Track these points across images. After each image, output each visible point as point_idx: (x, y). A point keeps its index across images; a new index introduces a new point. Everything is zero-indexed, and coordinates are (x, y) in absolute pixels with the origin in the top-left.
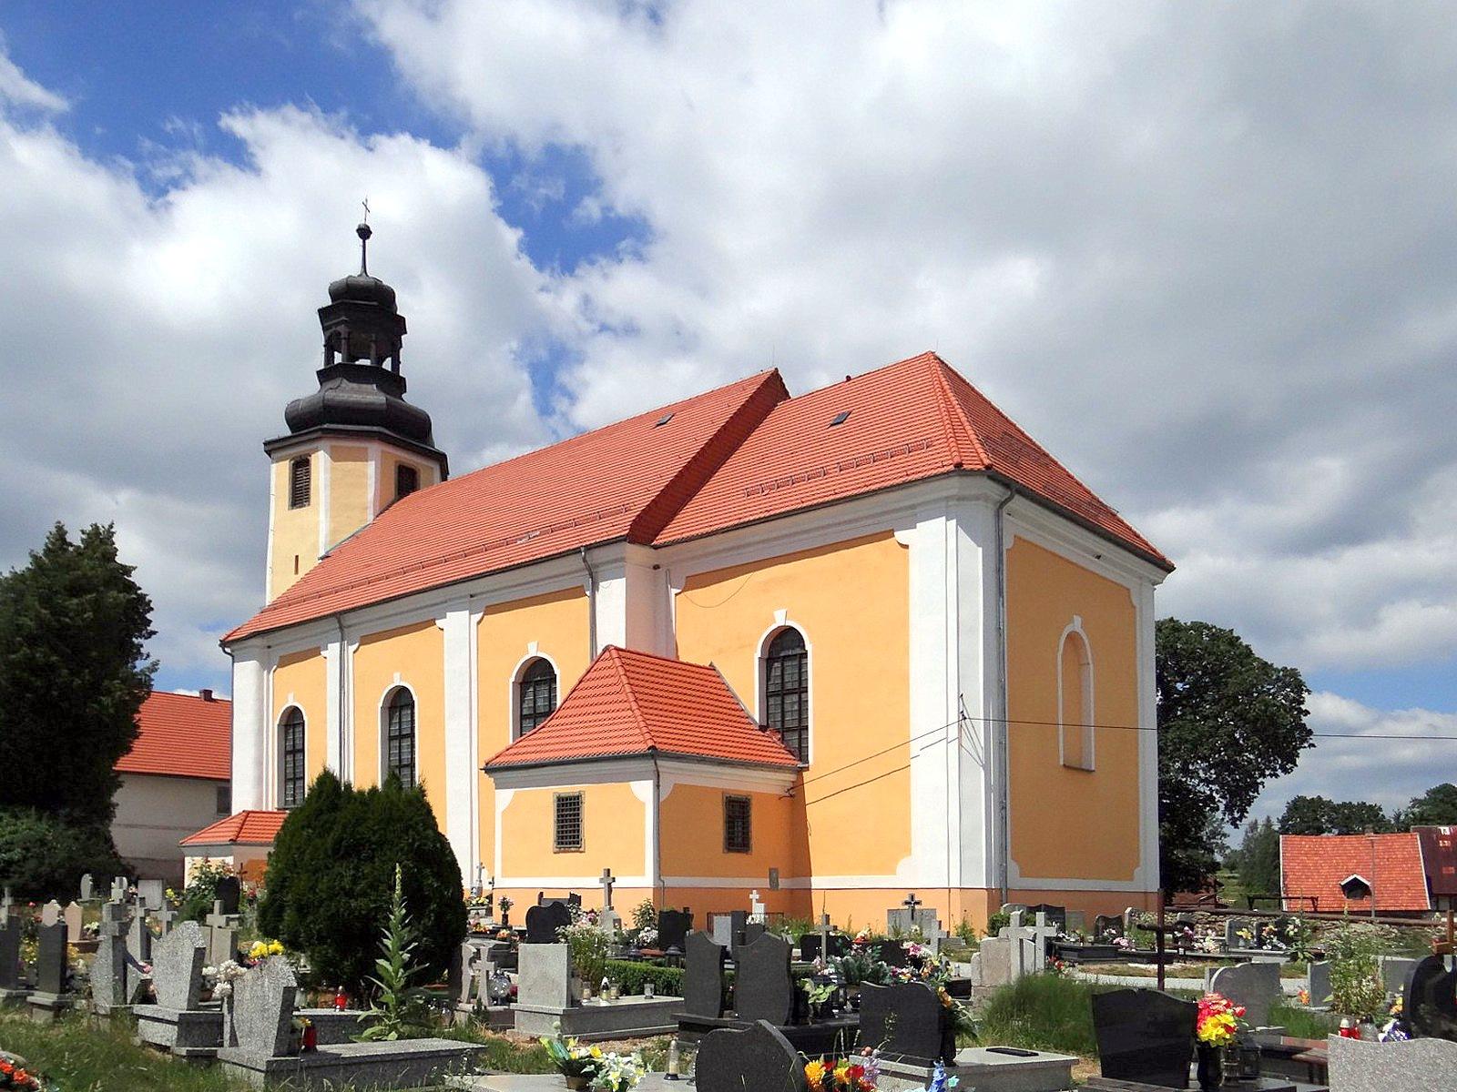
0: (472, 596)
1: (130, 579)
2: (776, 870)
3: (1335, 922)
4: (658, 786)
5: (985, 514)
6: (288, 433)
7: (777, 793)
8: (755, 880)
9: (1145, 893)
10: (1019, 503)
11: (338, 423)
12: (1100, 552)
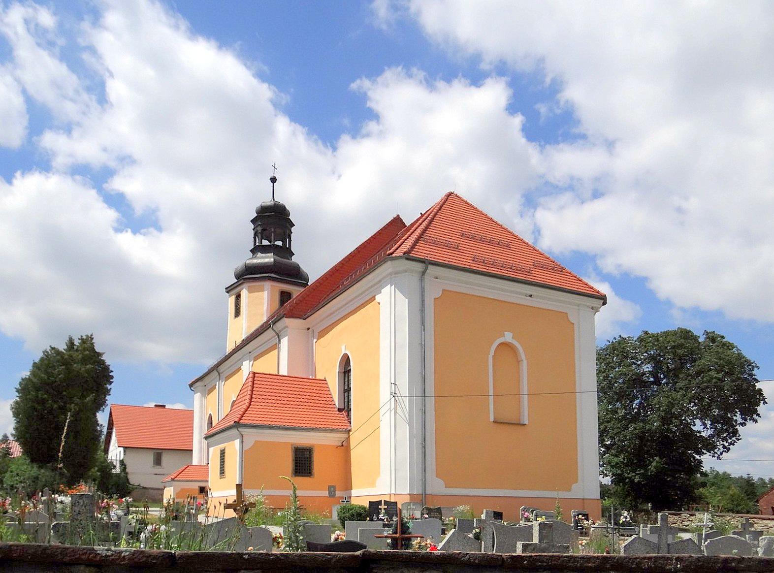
0: (250, 353)
1: (102, 358)
2: (334, 487)
3: (754, 520)
4: (242, 442)
5: (414, 280)
6: (236, 281)
7: (335, 444)
8: (320, 492)
9: (583, 499)
10: (432, 269)
11: (263, 273)
12: (531, 293)
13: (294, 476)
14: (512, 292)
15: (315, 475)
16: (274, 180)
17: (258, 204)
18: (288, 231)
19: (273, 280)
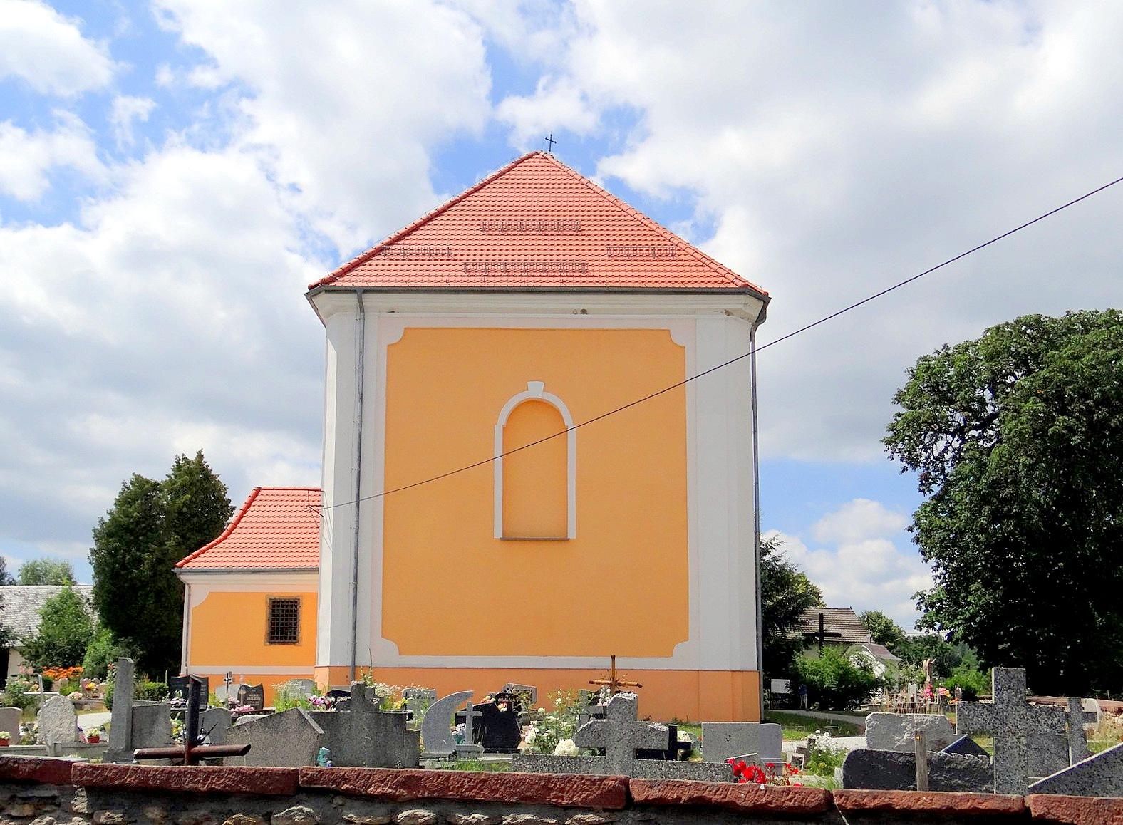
13: (268, 644)
14: (545, 311)
15: (303, 642)
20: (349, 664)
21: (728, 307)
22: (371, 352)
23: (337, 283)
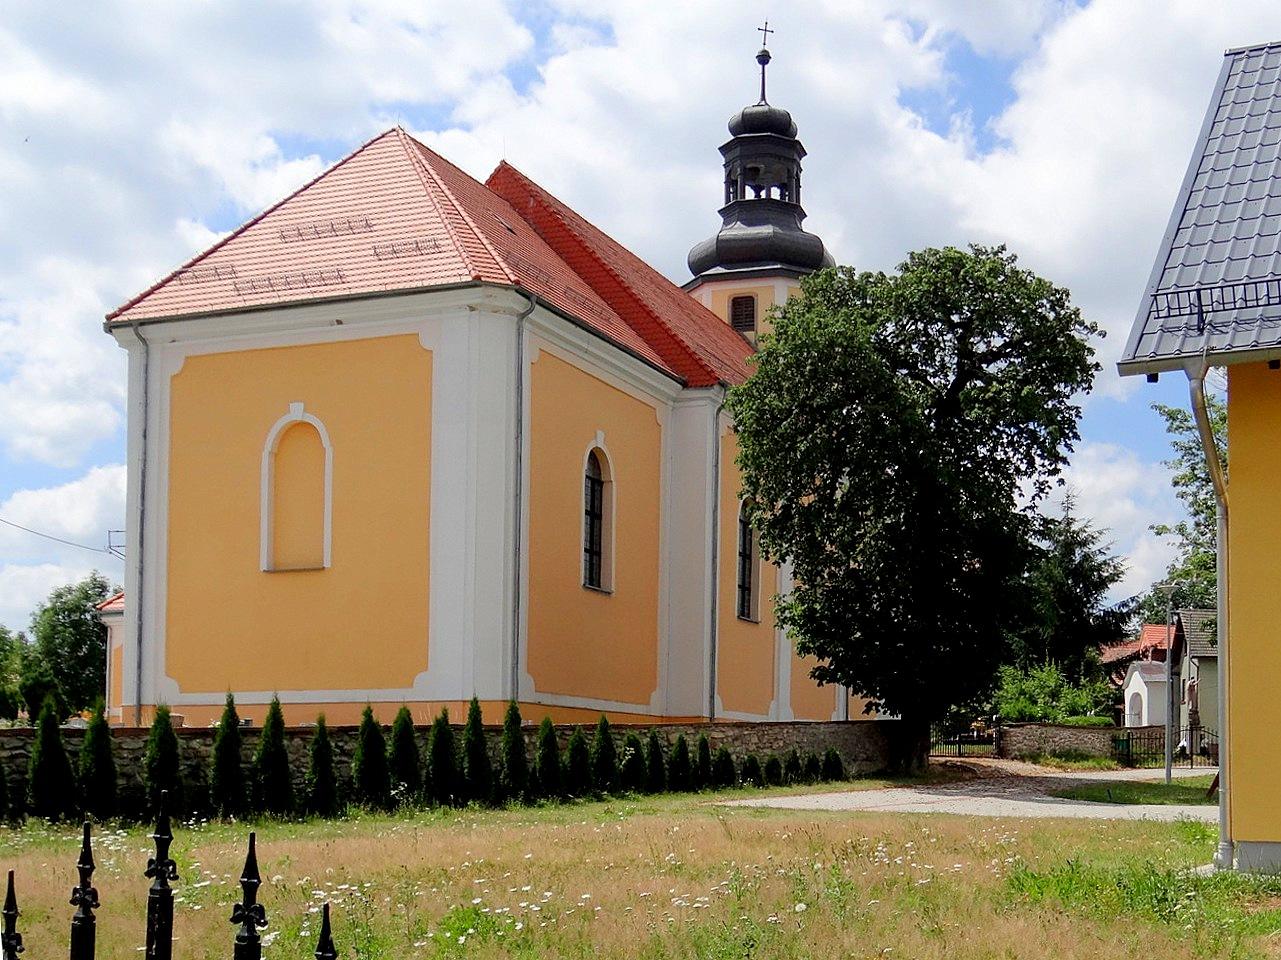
6: (694, 277)
10: (540, 315)
16: (764, 58)
17: (735, 112)
18: (795, 169)
19: (717, 281)
20: (135, 702)
21: (473, 302)
22: (154, 386)
23: (120, 319)
